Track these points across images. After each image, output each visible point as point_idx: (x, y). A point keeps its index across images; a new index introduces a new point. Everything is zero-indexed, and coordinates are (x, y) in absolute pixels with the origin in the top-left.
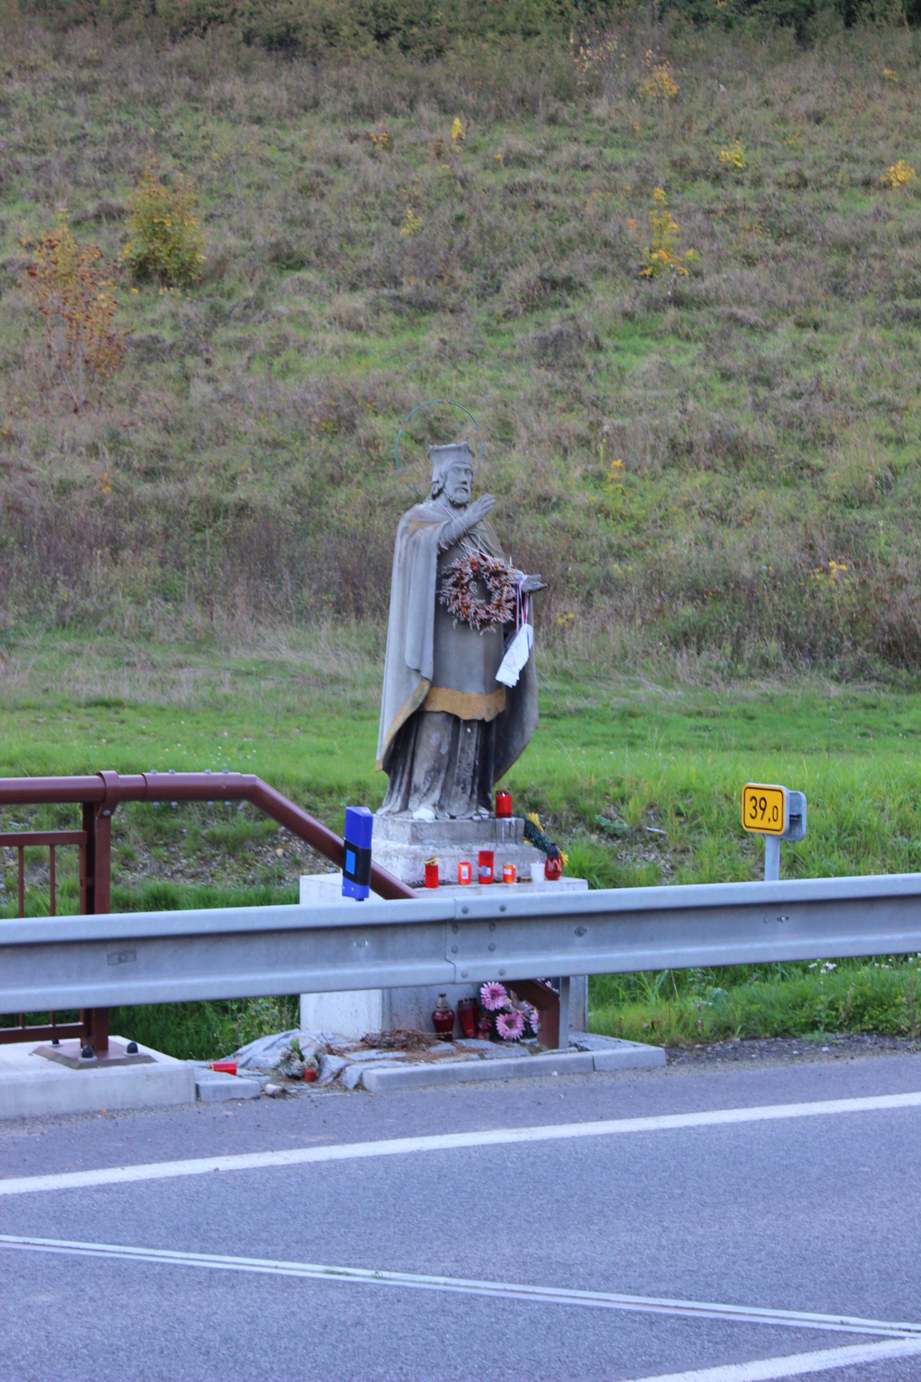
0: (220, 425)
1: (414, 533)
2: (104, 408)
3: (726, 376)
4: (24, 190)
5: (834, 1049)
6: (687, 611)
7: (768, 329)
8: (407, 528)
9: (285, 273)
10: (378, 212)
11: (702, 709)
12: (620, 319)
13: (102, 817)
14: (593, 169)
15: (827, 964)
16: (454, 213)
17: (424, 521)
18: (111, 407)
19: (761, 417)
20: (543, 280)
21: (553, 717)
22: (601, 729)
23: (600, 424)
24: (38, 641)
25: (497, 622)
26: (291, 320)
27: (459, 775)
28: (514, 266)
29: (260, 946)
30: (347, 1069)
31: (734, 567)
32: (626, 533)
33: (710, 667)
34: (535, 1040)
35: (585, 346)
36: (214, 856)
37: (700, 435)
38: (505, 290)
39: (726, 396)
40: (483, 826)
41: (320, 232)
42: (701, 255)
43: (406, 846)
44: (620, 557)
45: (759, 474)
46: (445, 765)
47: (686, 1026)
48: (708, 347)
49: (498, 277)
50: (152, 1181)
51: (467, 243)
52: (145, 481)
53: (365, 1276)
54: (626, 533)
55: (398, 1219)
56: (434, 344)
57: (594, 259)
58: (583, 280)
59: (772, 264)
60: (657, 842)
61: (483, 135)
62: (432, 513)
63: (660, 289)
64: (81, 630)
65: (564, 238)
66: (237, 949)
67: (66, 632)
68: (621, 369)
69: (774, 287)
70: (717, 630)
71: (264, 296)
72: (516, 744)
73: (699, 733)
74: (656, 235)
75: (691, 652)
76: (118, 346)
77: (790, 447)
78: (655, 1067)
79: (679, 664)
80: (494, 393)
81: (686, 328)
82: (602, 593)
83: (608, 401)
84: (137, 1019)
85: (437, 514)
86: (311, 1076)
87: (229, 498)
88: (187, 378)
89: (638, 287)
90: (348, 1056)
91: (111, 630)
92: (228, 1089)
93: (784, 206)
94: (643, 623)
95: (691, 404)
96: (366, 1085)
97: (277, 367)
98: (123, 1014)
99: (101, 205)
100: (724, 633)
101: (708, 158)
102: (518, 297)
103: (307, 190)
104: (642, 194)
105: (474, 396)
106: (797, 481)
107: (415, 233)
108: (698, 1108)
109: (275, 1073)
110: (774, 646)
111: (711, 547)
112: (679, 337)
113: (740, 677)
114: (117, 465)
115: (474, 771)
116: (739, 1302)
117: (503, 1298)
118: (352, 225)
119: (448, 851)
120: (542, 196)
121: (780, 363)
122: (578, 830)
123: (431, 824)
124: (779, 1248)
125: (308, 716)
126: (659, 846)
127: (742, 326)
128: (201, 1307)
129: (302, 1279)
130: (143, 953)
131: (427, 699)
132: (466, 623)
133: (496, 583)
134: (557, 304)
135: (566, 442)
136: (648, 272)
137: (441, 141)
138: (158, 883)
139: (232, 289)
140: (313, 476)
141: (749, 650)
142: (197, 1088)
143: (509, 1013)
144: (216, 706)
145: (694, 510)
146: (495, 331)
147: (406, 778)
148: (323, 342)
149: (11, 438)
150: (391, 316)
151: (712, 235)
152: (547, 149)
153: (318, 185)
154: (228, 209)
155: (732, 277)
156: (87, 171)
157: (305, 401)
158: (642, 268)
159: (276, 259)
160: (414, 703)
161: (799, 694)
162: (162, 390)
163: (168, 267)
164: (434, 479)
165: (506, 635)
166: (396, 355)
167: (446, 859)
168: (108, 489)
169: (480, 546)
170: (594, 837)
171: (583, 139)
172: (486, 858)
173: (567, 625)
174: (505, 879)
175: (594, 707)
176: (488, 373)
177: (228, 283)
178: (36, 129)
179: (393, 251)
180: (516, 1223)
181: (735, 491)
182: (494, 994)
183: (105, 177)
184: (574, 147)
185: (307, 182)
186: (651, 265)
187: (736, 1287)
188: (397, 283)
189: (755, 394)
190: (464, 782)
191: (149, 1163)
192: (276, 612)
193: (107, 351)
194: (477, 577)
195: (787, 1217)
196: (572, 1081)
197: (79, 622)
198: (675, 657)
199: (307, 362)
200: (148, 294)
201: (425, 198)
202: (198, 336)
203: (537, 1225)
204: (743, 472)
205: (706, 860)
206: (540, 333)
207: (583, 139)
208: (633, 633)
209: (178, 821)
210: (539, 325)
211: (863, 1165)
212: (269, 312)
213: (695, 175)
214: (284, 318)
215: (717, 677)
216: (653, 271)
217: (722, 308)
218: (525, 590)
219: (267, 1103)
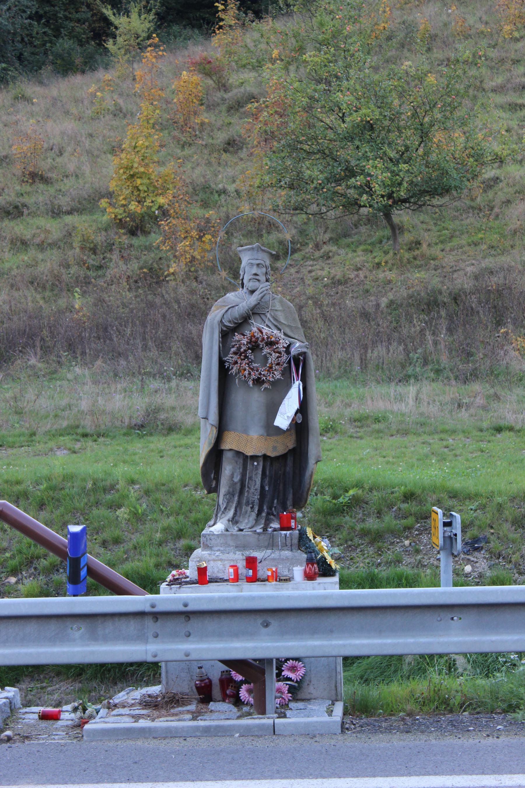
46: (238, 491)
160: (210, 444)
167: (226, 562)
169: (267, 322)
174: (267, 580)
190: (253, 503)
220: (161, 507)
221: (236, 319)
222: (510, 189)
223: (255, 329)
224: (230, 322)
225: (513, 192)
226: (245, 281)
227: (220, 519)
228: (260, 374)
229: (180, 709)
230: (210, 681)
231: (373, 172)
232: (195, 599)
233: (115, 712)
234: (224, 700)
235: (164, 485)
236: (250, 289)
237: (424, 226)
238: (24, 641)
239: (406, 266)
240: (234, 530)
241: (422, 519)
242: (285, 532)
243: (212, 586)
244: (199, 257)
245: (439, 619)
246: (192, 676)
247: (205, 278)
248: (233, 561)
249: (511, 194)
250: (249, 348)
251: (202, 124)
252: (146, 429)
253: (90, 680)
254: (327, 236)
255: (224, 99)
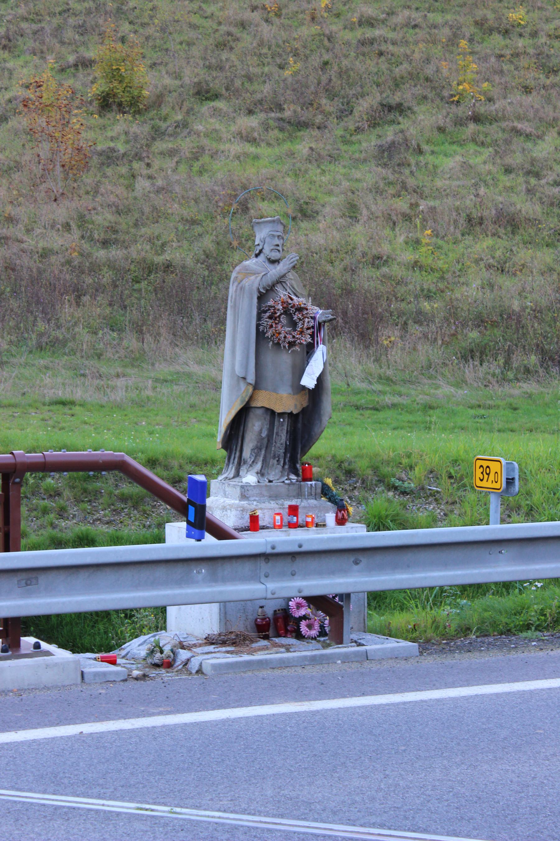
0: (155, 209)
1: (241, 281)
2: (75, 198)
3: (508, 170)
4: (26, 48)
5: (541, 643)
6: (474, 335)
7: (538, 137)
8: (237, 277)
9: (204, 103)
10: (269, 60)
11: (481, 403)
12: (436, 132)
13: (14, 483)
14: (420, 27)
15: (537, 584)
16: (322, 59)
17: (248, 272)
18: (81, 197)
19: (531, 199)
20: (382, 105)
21: (375, 409)
22: (411, 418)
23: (417, 205)
24: (23, 360)
25: (301, 344)
26: (207, 135)
27: (275, 452)
28: (363, 96)
29: (127, 573)
30: (192, 659)
31: (507, 303)
32: (435, 281)
33: (489, 374)
34: (327, 638)
35: (411, 150)
36: (123, 509)
37: (488, 211)
38: (356, 113)
39: (508, 184)
40: (291, 487)
41: (229, 74)
42: (493, 86)
43: (237, 502)
44: (429, 297)
45: (529, 239)
46: (265, 445)
47: (437, 627)
48: (496, 150)
49: (352, 104)
50: (34, 741)
51: (330, 80)
52: (103, 248)
53: (164, 812)
54: (435, 281)
55: (199, 769)
56: (306, 151)
57: (419, 90)
58: (411, 104)
59: (543, 92)
60: (435, 497)
61: (345, 5)
62: (255, 267)
63: (463, 111)
64: (54, 352)
65: (398, 76)
66: (110, 576)
67: (43, 353)
68: (435, 167)
69: (543, 107)
70: (494, 348)
71: (189, 120)
72: (316, 430)
73: (477, 420)
74: (461, 73)
75: (476, 363)
76: (85, 155)
77: (551, 219)
78: (411, 657)
79: (467, 371)
80: (346, 184)
81: (482, 137)
82: (415, 322)
83: (425, 189)
84: (64, 622)
85: (258, 268)
86: (168, 665)
87: (159, 259)
88: (134, 176)
89: (449, 110)
90: (194, 650)
91: (73, 352)
92: (104, 674)
93: (552, 51)
94: (442, 343)
95: (482, 191)
96: (204, 671)
97: (196, 168)
98: (54, 619)
99: (78, 57)
100: (499, 350)
101: (500, 19)
102: (365, 117)
103: (221, 46)
104: (453, 45)
105: (332, 187)
106: (556, 243)
107: (296, 73)
108: (434, 687)
109: (145, 662)
110: (533, 359)
111: (492, 291)
112: (477, 143)
113: (510, 381)
114: (83, 237)
115: (286, 449)
116: (425, 831)
117: (257, 828)
118: (251, 69)
119: (267, 505)
120: (383, 48)
121: (546, 161)
122: (381, 488)
123: (254, 486)
124: (463, 790)
125: (205, 411)
126: (436, 500)
127: (520, 135)
128: (40, 835)
129: (118, 814)
130: (43, 579)
131: (251, 398)
132: (278, 344)
133: (300, 316)
134: (393, 122)
135: (394, 218)
136: (456, 99)
137: (315, 10)
138: (83, 528)
139: (167, 114)
140: (218, 244)
141: (517, 360)
142: (82, 673)
143: (309, 619)
144: (140, 404)
145: (482, 264)
146: (349, 141)
147: (238, 454)
148: (229, 151)
149: (10, 220)
150: (276, 131)
151: (502, 72)
152: (388, 14)
153: (229, 41)
154: (166, 59)
155: (514, 102)
156: (69, 34)
157: (213, 191)
158: (452, 96)
159: (198, 93)
160: (242, 402)
161: (550, 392)
162: (115, 184)
163: (123, 100)
164: (256, 243)
165: (308, 353)
166: (279, 158)
167: (266, 511)
168: (76, 254)
170: (391, 494)
171: (413, 7)
172: (293, 510)
173: (390, 346)
174: (307, 525)
175: (405, 402)
176: (343, 171)
177: (165, 110)
178: (35, 5)
179: (279, 87)
180: (282, 772)
181: (511, 250)
182: (299, 606)
183: (81, 38)
184: (407, 13)
185: (221, 39)
186: (458, 94)
187: (425, 820)
188: (281, 109)
189: (527, 182)
191: (36, 728)
192: (188, 338)
193: (76, 158)
194: (286, 312)
195: (475, 767)
196: (350, 667)
197: (52, 346)
198: (464, 367)
199: (217, 165)
200: (109, 119)
201: (303, 50)
202: (142, 147)
203: (296, 773)
204: (518, 238)
205: (468, 510)
206: (379, 142)
207: (413, 7)
208: (435, 350)
209: (99, 484)
210: (380, 136)
211: (540, 728)
212: (192, 130)
213: (491, 31)
214: (202, 134)
215: (493, 381)
216: (459, 98)
217: (507, 123)
218: (320, 321)
219: (131, 684)
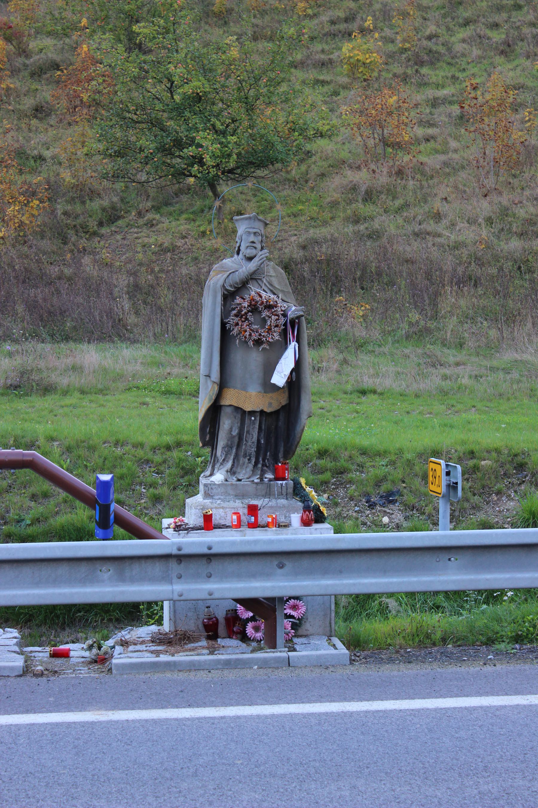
29: (27, 570)
123: (219, 485)
160: (210, 400)
167: (227, 510)
169: (264, 287)
174: (267, 525)
190: (250, 455)
220: (85, 463)
221: (237, 283)
222: (324, 163)
223: (253, 293)
224: (231, 286)
225: (326, 166)
226: (242, 248)
227: (219, 470)
228: (260, 335)
229: (192, 645)
230: (217, 620)
231: (205, 143)
232: (218, 543)
233: (131, 648)
234: (230, 637)
235: (84, 442)
236: (247, 256)
237: (244, 197)
238: (56, 582)
239: (230, 235)
240: (233, 480)
241: (338, 474)
242: (281, 482)
243: (217, 531)
244: (27, 222)
245: (438, 560)
246: (198, 615)
247: (35, 242)
248: (234, 508)
249: (325, 168)
250: (249, 311)
251: (8, 89)
252: (23, 389)
253: (39, 626)
254: (149, 204)
255: (25, 65)
